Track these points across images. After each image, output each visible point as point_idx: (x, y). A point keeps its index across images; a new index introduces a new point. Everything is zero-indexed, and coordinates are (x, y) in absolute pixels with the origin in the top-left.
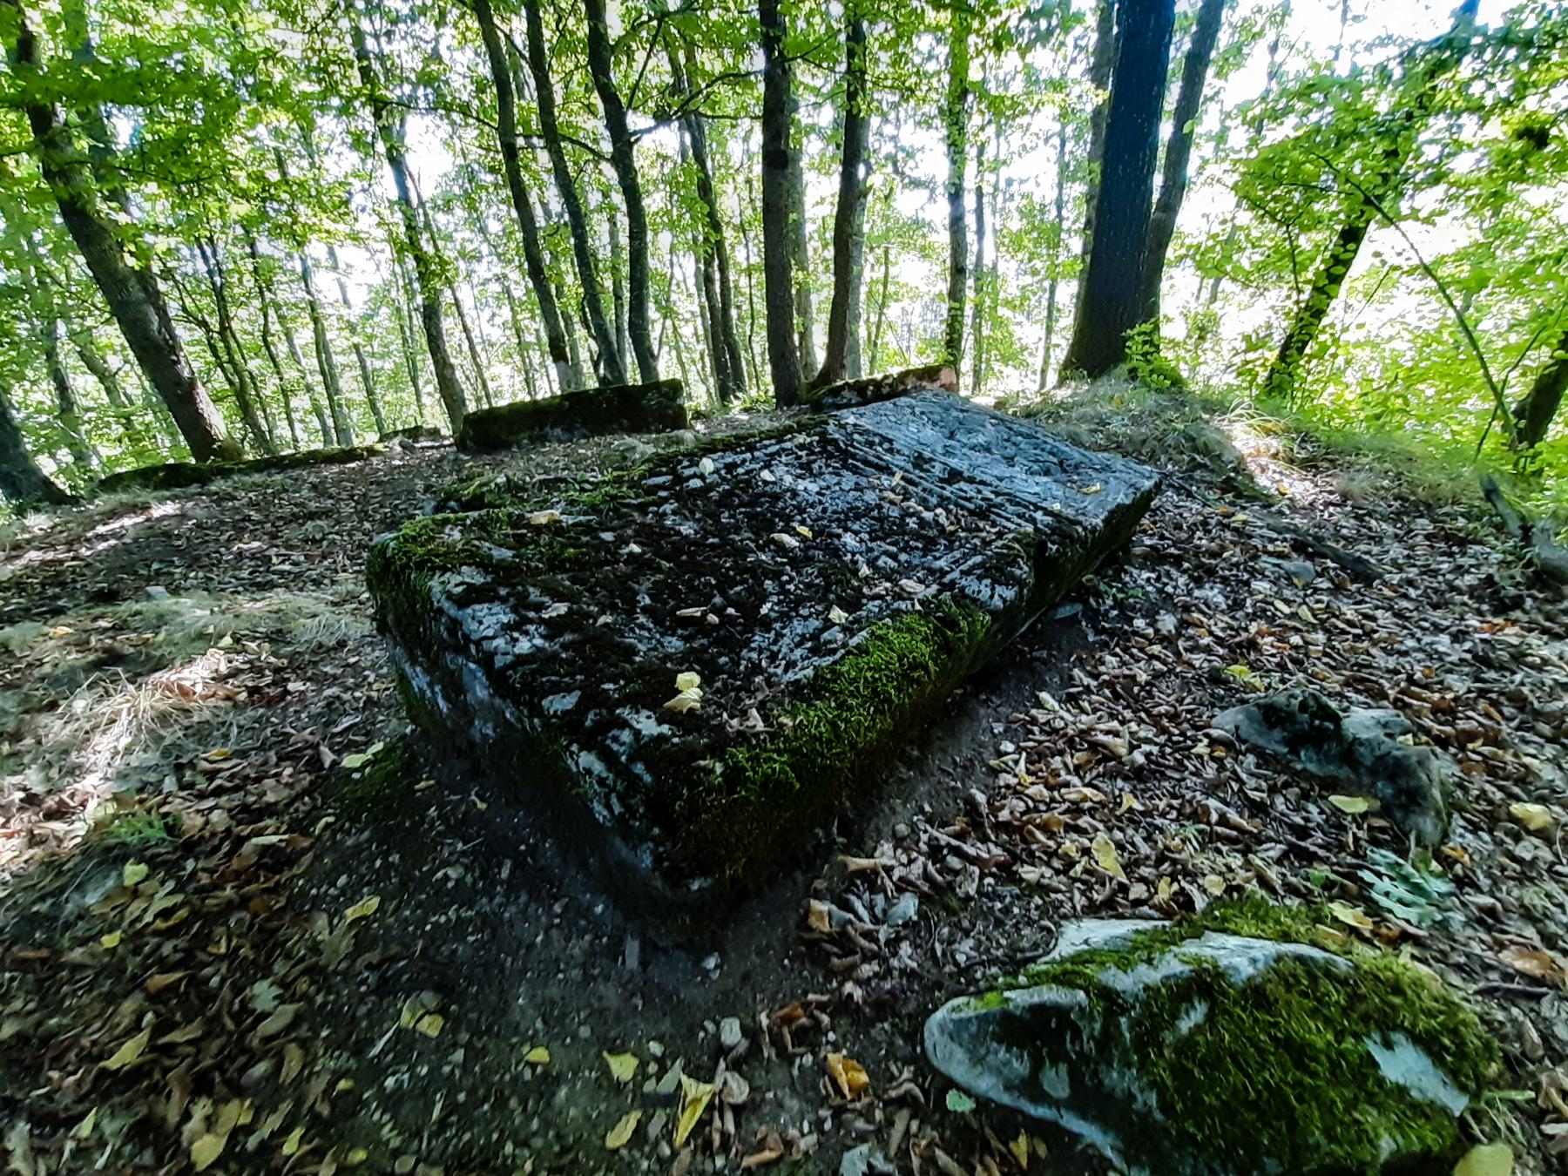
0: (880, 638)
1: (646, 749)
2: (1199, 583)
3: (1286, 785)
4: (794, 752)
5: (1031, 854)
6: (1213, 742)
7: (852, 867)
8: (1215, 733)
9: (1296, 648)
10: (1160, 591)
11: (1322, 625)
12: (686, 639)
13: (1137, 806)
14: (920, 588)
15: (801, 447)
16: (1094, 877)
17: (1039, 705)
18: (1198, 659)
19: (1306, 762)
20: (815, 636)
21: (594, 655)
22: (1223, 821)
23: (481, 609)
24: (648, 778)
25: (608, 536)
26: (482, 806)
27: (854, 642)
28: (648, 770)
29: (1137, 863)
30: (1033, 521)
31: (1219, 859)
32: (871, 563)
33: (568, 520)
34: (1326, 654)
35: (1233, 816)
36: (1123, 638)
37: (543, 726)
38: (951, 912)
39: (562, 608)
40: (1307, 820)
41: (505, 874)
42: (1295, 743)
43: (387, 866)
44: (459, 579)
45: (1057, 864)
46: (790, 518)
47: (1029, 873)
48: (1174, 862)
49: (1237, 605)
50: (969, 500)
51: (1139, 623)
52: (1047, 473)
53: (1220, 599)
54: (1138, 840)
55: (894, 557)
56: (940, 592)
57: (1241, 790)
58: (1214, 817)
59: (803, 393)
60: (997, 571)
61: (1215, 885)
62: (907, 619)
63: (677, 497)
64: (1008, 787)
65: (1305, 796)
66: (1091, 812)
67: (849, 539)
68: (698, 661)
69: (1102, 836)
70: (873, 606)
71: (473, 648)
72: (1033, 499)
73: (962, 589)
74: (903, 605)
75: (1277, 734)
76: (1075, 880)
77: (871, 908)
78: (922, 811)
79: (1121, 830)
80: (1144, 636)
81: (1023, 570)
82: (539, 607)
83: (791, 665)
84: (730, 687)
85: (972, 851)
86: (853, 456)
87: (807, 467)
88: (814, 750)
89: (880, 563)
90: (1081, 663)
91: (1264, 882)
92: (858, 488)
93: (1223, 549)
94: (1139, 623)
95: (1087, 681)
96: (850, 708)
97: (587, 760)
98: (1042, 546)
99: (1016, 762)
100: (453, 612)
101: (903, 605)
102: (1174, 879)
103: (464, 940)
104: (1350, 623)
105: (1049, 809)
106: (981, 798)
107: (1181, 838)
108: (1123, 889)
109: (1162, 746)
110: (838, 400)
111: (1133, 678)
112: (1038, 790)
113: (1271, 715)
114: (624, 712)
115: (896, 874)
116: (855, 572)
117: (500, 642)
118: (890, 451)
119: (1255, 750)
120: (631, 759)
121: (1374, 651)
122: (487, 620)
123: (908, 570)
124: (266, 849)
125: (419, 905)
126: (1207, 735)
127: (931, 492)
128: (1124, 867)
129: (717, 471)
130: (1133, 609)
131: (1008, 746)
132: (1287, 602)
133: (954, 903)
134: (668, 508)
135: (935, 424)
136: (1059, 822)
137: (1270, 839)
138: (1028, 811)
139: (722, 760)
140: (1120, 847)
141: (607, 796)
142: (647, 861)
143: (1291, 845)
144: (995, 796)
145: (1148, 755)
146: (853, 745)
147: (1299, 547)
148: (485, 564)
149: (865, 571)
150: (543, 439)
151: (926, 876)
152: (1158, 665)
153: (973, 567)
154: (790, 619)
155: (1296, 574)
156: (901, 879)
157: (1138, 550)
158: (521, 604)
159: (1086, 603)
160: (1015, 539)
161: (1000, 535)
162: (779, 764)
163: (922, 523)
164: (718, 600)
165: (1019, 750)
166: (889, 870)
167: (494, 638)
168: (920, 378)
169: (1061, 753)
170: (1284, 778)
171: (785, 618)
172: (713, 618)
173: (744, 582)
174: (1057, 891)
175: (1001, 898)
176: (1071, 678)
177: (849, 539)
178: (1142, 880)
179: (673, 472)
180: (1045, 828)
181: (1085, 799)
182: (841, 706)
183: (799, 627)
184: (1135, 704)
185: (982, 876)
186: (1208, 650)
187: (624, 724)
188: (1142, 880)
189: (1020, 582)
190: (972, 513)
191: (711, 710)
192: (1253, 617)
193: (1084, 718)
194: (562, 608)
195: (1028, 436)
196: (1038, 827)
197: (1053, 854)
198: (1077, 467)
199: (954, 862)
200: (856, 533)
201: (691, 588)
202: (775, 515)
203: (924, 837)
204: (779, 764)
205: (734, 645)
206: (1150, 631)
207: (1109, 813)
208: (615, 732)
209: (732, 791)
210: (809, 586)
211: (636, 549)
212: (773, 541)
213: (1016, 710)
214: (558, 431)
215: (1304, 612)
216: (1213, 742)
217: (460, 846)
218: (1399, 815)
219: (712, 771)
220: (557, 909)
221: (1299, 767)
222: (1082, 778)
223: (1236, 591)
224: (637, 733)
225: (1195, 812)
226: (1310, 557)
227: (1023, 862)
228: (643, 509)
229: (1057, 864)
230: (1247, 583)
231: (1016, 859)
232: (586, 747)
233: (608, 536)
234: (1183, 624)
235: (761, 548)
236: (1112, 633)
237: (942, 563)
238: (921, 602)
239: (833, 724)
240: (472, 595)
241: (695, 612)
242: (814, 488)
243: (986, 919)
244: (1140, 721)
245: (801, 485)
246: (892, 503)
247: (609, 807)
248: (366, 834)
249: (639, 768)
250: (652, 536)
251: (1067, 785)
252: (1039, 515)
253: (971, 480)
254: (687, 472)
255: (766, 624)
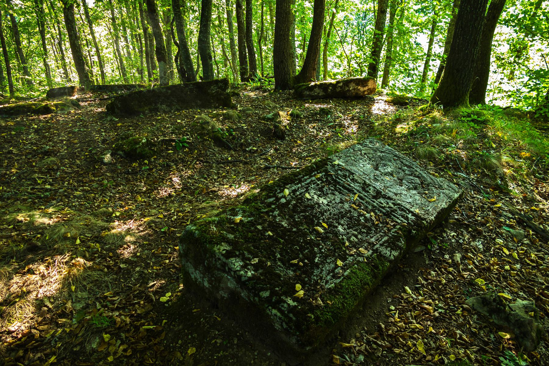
0: (355, 273)
1: (292, 309)
2: (474, 238)
3: (485, 327)
4: (332, 312)
5: (398, 345)
6: (464, 309)
7: (344, 346)
8: (465, 306)
9: (506, 271)
10: (457, 241)
11: (521, 261)
12: (294, 271)
13: (433, 331)
14: (366, 252)
15: (319, 179)
16: (416, 353)
17: (405, 291)
18: (466, 274)
19: (494, 319)
20: (333, 271)
21: (268, 277)
22: (461, 338)
23: (233, 260)
24: (294, 318)
25: (259, 227)
26: (219, 319)
27: (346, 274)
28: (294, 315)
29: (430, 350)
30: (407, 218)
31: (456, 350)
32: (348, 239)
33: (245, 220)
34: (517, 274)
35: (464, 337)
36: (439, 263)
37: (259, 300)
38: (374, 360)
39: (256, 260)
40: (489, 339)
41: (236, 342)
42: (492, 312)
43: (193, 338)
44: (222, 248)
45: (405, 348)
46: (318, 219)
47: (397, 351)
48: (442, 350)
49: (487, 249)
50: (383, 208)
51: (447, 256)
52: (415, 188)
53: (481, 246)
54: (431, 342)
55: (356, 236)
56: (373, 253)
57: (469, 328)
58: (458, 336)
59: (291, 83)
60: (392, 244)
61: (453, 358)
62: (362, 265)
63: (278, 207)
64: (392, 322)
65: (491, 331)
66: (418, 333)
67: (340, 228)
68: (300, 280)
69: (420, 341)
70: (350, 259)
71: (232, 273)
72: (408, 206)
73: (380, 252)
74: (361, 259)
75: (486, 309)
76: (411, 353)
77: (350, 358)
78: (364, 329)
79: (427, 339)
80: (448, 263)
81: (402, 243)
82: (250, 260)
83: (327, 282)
84: (312, 288)
85: (380, 343)
86: (339, 183)
87: (321, 190)
88: (338, 312)
89: (352, 239)
90: (422, 274)
91: (469, 358)
92: (342, 202)
93: (487, 222)
94: (447, 256)
95: (423, 282)
96: (347, 299)
97: (274, 311)
98: (410, 232)
99: (395, 314)
100: (224, 260)
101: (361, 259)
102: (440, 355)
103: (228, 361)
104: (532, 261)
105: (405, 331)
106: (383, 326)
107: (445, 342)
108: (425, 357)
109: (446, 310)
110: (312, 93)
111: (440, 281)
112: (401, 324)
113: (485, 302)
114: (283, 297)
115: (357, 348)
116: (344, 243)
117: (242, 272)
118: (353, 180)
119: (478, 314)
120: (289, 312)
121: (538, 274)
122: (237, 264)
123: (360, 243)
124: (147, 330)
125: (210, 350)
126: (462, 307)
127: (369, 203)
128: (426, 351)
129: (289, 194)
130: (445, 250)
131: (393, 308)
132: (509, 249)
133: (375, 358)
134: (276, 213)
135: (370, 159)
136: (407, 335)
137: (475, 345)
138: (398, 331)
139: (313, 314)
140: (425, 344)
141: (282, 323)
142: (294, 341)
143: (481, 348)
144: (387, 325)
145: (440, 313)
146: (348, 311)
147: (520, 222)
148: (228, 242)
149: (347, 244)
150: (156, 110)
151: (366, 349)
152: (451, 276)
153: (384, 242)
154: (324, 263)
155: (516, 236)
156: (358, 350)
157: (451, 221)
158: (244, 259)
159: (427, 246)
160: (400, 229)
161: (394, 226)
162: (329, 316)
163: (366, 219)
164: (301, 256)
165: (396, 309)
166: (355, 347)
167: (240, 271)
168: (358, 84)
169: (410, 311)
170: (485, 324)
171: (323, 263)
172: (301, 264)
173: (307, 248)
174: (406, 356)
175: (388, 357)
176: (417, 280)
177: (340, 228)
178: (431, 355)
179: (275, 196)
180: (402, 337)
181: (417, 328)
182: (344, 297)
183: (327, 267)
184: (440, 293)
185: (383, 351)
186: (471, 270)
187: (285, 302)
188: (431, 355)
189: (400, 248)
190: (384, 214)
191: (306, 297)
192: (492, 256)
193: (420, 298)
194: (256, 260)
195: (409, 167)
196: (401, 337)
197: (405, 345)
198: (428, 185)
199: (374, 346)
200: (342, 225)
201: (292, 251)
202: (314, 216)
203: (365, 338)
204: (329, 316)
205: (309, 274)
206: (450, 261)
207: (424, 334)
208: (282, 304)
209: (317, 324)
210: (329, 250)
211: (271, 234)
212: (315, 230)
213: (396, 293)
214: (164, 106)
215: (515, 255)
216: (464, 309)
217: (217, 332)
218: (521, 340)
219: (311, 317)
220: (256, 354)
221: (491, 321)
222: (416, 321)
223: (489, 243)
224: (289, 305)
225: (452, 334)
226: (524, 228)
227: (395, 347)
228: (267, 213)
229: (405, 348)
230: (494, 239)
231: (393, 346)
232: (274, 308)
233: (259, 227)
234: (463, 258)
235: (311, 233)
236: (435, 260)
237: (373, 240)
238: (367, 258)
239: (343, 304)
240: (229, 254)
241: (295, 261)
242: (325, 202)
243: (384, 363)
244: (440, 300)
245: (322, 200)
246: (354, 209)
247: (282, 326)
248: (181, 327)
249: (291, 315)
250: (274, 226)
251: (411, 323)
252: (410, 216)
253: (385, 197)
254: (280, 195)
255: (317, 266)
